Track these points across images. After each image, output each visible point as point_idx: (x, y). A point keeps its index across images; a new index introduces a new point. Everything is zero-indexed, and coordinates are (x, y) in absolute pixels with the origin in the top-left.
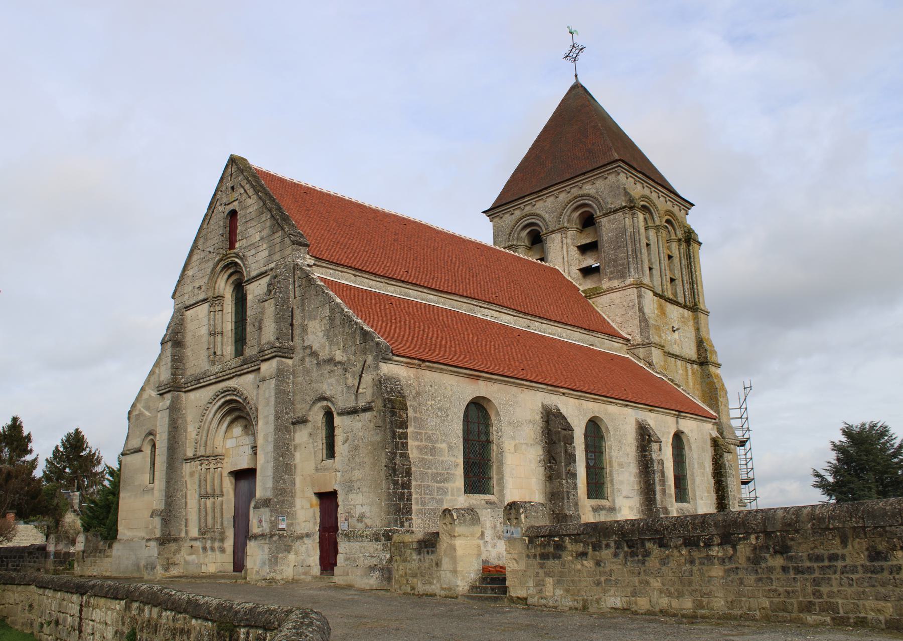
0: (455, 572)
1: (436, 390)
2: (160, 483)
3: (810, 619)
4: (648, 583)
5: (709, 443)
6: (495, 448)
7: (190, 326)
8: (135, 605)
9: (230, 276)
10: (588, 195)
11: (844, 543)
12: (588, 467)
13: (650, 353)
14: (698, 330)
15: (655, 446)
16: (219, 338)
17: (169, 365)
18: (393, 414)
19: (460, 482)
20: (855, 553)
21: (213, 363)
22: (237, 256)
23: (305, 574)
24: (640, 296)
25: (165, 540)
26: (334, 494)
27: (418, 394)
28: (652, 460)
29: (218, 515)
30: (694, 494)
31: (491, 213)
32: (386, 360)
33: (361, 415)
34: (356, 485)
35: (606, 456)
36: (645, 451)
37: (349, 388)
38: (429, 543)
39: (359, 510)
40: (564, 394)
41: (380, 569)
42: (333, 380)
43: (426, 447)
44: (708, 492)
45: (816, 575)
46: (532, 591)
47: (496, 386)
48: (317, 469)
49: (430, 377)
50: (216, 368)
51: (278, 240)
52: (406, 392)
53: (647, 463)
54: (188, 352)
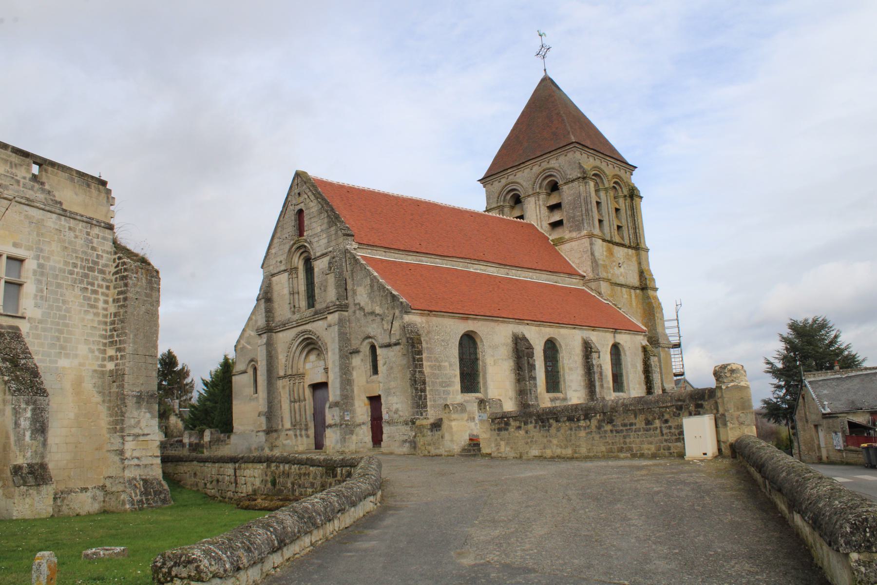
0: (452, 441)
3: (622, 455)
4: (551, 441)
5: (640, 349)
7: (276, 288)
8: (273, 465)
10: (553, 168)
11: (635, 417)
12: (547, 372)
13: (599, 286)
14: (640, 264)
15: (595, 355)
16: (296, 296)
17: (264, 315)
18: (413, 346)
19: (458, 386)
20: (640, 422)
21: (294, 313)
22: (306, 241)
23: (363, 447)
24: (591, 244)
25: (269, 431)
27: (429, 332)
28: (593, 365)
29: (303, 413)
30: (628, 386)
32: (407, 313)
34: (392, 391)
35: (560, 364)
37: (385, 330)
38: (437, 425)
39: (395, 407)
41: (410, 442)
42: (375, 326)
43: (435, 365)
44: (640, 384)
45: (625, 433)
46: (494, 449)
47: (480, 323)
48: (367, 382)
49: (563, 331)
50: (297, 316)
51: (333, 232)
52: (421, 332)
54: (276, 305)
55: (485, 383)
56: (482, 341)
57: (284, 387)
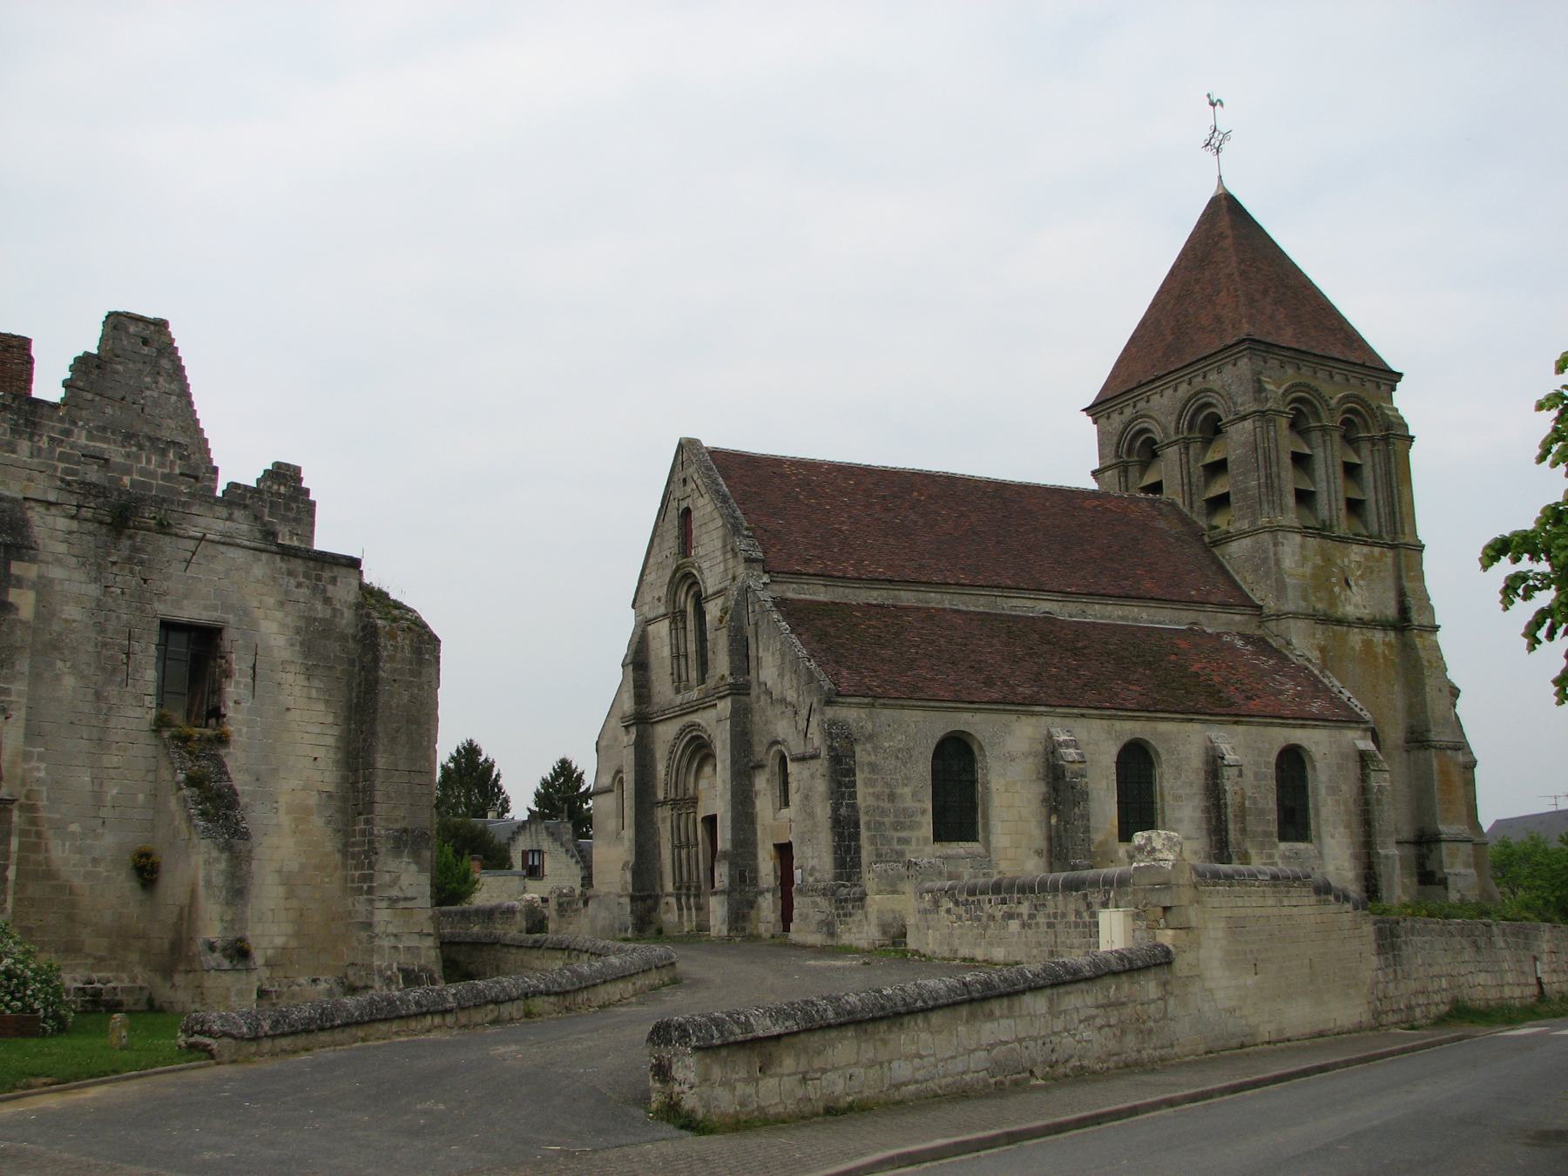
2: (629, 833)
7: (654, 645)
10: (1210, 390)
19: (927, 829)
21: (678, 691)
26: (789, 845)
47: (979, 717)
49: (1163, 727)
55: (986, 825)
56: (981, 748)
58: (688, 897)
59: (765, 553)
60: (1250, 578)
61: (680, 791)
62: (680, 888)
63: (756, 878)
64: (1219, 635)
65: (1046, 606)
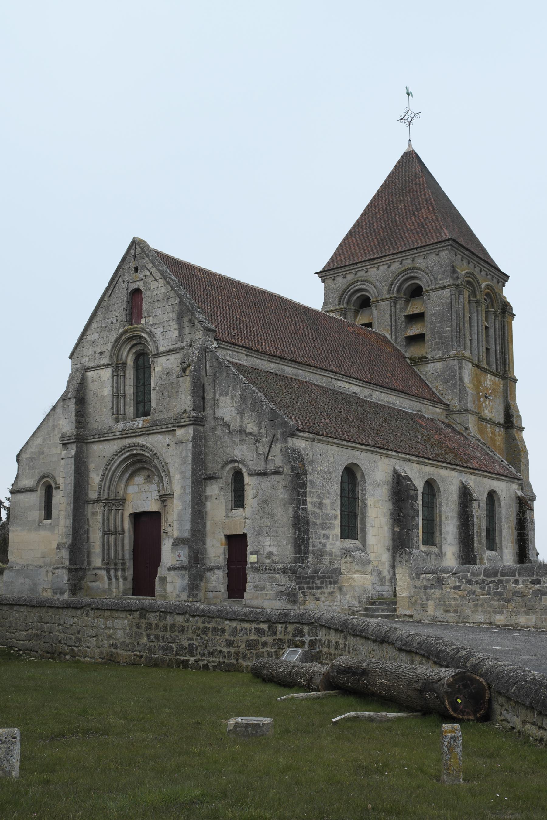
1: (323, 458)
6: (360, 504)
7: (92, 387)
9: (133, 346)
19: (337, 531)
22: (144, 331)
26: (243, 537)
31: (323, 274)
32: (292, 435)
33: (270, 477)
34: (264, 531)
36: (467, 507)
39: (268, 549)
40: (409, 460)
42: (244, 448)
44: (512, 543)
47: (364, 455)
48: (227, 516)
49: (320, 447)
50: (120, 426)
53: (468, 517)
55: (364, 530)
56: (363, 476)
57: (94, 514)
58: (116, 570)
59: (217, 326)
60: (440, 387)
61: (112, 493)
62: (108, 564)
63: (203, 559)
64: (432, 420)
65: (355, 389)
